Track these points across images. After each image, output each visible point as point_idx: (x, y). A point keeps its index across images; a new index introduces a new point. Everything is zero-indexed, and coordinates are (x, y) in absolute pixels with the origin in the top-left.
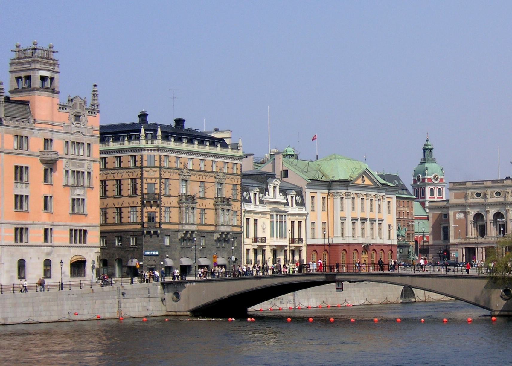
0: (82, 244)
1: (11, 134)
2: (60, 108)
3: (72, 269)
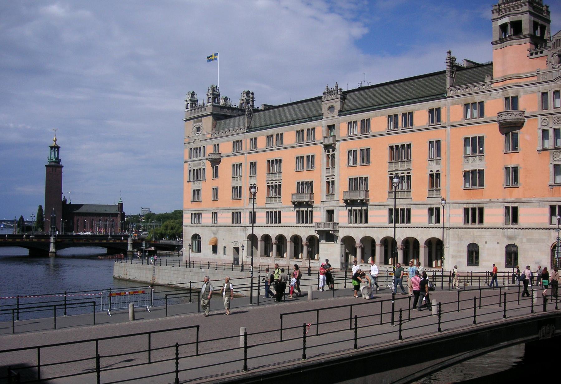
0: (477, 225)
1: (459, 104)
2: (532, 54)
3: (415, 252)
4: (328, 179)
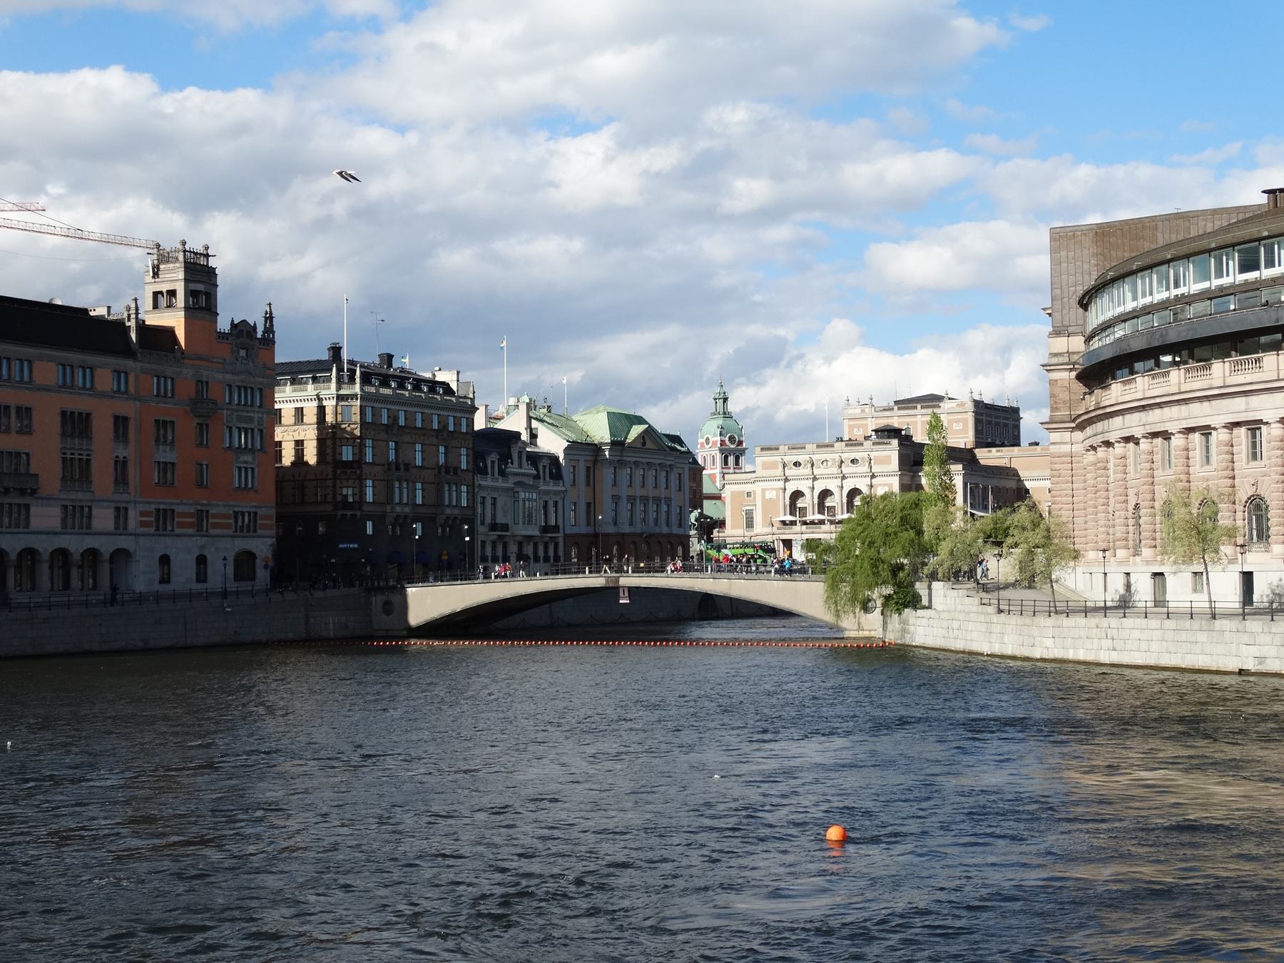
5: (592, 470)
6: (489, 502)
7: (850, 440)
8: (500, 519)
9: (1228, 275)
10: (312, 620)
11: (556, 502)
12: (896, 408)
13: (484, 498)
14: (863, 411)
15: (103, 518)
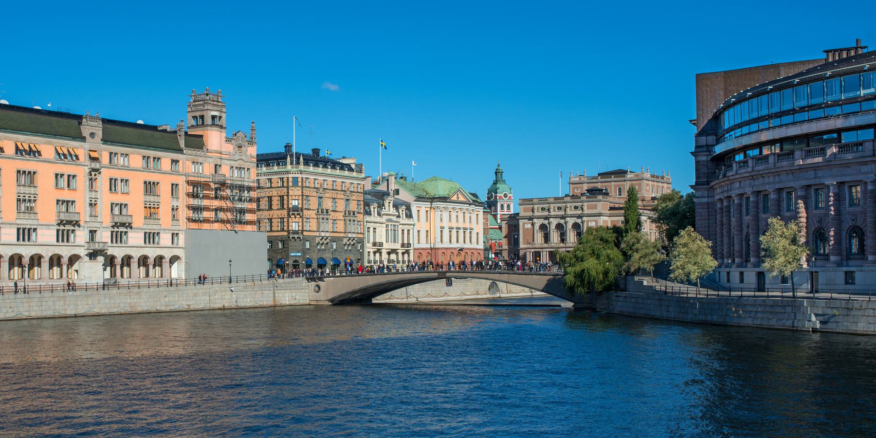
4: (91, 201)
5: (429, 212)
6: (371, 230)
7: (573, 195)
8: (377, 241)
9: (804, 100)
10: (277, 295)
11: (408, 230)
12: (599, 177)
13: (369, 228)
14: (580, 179)
15: (165, 239)
